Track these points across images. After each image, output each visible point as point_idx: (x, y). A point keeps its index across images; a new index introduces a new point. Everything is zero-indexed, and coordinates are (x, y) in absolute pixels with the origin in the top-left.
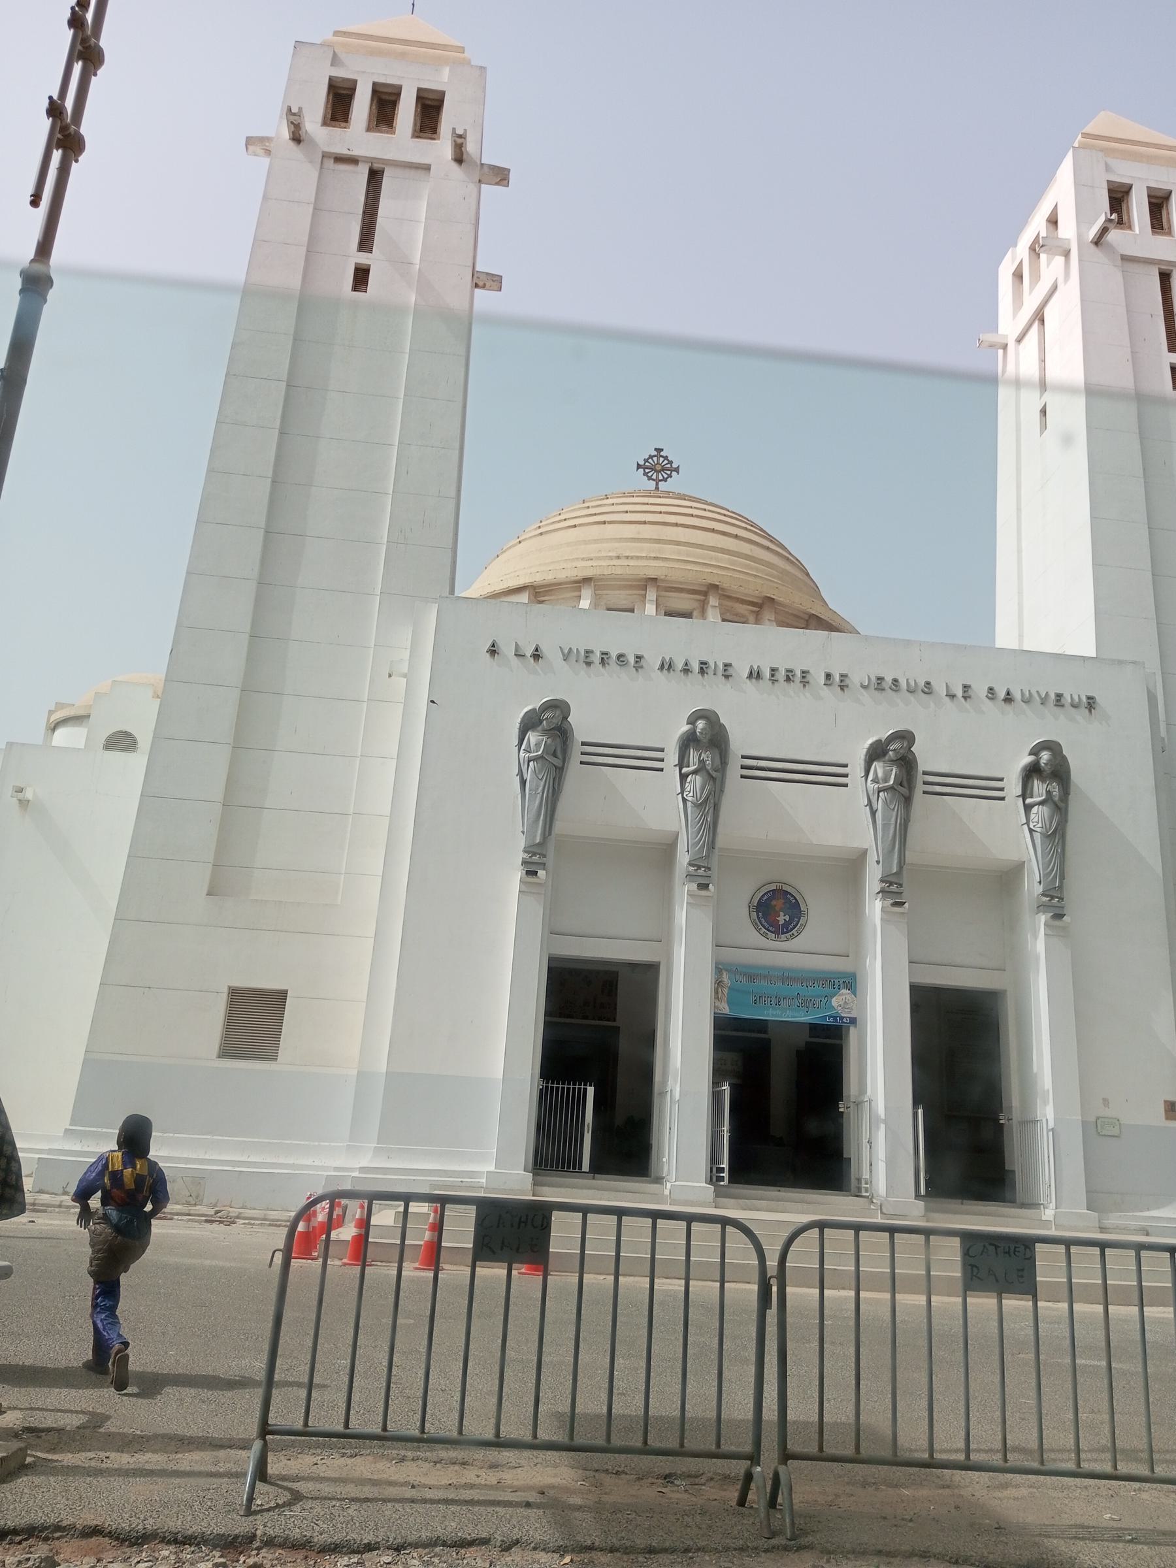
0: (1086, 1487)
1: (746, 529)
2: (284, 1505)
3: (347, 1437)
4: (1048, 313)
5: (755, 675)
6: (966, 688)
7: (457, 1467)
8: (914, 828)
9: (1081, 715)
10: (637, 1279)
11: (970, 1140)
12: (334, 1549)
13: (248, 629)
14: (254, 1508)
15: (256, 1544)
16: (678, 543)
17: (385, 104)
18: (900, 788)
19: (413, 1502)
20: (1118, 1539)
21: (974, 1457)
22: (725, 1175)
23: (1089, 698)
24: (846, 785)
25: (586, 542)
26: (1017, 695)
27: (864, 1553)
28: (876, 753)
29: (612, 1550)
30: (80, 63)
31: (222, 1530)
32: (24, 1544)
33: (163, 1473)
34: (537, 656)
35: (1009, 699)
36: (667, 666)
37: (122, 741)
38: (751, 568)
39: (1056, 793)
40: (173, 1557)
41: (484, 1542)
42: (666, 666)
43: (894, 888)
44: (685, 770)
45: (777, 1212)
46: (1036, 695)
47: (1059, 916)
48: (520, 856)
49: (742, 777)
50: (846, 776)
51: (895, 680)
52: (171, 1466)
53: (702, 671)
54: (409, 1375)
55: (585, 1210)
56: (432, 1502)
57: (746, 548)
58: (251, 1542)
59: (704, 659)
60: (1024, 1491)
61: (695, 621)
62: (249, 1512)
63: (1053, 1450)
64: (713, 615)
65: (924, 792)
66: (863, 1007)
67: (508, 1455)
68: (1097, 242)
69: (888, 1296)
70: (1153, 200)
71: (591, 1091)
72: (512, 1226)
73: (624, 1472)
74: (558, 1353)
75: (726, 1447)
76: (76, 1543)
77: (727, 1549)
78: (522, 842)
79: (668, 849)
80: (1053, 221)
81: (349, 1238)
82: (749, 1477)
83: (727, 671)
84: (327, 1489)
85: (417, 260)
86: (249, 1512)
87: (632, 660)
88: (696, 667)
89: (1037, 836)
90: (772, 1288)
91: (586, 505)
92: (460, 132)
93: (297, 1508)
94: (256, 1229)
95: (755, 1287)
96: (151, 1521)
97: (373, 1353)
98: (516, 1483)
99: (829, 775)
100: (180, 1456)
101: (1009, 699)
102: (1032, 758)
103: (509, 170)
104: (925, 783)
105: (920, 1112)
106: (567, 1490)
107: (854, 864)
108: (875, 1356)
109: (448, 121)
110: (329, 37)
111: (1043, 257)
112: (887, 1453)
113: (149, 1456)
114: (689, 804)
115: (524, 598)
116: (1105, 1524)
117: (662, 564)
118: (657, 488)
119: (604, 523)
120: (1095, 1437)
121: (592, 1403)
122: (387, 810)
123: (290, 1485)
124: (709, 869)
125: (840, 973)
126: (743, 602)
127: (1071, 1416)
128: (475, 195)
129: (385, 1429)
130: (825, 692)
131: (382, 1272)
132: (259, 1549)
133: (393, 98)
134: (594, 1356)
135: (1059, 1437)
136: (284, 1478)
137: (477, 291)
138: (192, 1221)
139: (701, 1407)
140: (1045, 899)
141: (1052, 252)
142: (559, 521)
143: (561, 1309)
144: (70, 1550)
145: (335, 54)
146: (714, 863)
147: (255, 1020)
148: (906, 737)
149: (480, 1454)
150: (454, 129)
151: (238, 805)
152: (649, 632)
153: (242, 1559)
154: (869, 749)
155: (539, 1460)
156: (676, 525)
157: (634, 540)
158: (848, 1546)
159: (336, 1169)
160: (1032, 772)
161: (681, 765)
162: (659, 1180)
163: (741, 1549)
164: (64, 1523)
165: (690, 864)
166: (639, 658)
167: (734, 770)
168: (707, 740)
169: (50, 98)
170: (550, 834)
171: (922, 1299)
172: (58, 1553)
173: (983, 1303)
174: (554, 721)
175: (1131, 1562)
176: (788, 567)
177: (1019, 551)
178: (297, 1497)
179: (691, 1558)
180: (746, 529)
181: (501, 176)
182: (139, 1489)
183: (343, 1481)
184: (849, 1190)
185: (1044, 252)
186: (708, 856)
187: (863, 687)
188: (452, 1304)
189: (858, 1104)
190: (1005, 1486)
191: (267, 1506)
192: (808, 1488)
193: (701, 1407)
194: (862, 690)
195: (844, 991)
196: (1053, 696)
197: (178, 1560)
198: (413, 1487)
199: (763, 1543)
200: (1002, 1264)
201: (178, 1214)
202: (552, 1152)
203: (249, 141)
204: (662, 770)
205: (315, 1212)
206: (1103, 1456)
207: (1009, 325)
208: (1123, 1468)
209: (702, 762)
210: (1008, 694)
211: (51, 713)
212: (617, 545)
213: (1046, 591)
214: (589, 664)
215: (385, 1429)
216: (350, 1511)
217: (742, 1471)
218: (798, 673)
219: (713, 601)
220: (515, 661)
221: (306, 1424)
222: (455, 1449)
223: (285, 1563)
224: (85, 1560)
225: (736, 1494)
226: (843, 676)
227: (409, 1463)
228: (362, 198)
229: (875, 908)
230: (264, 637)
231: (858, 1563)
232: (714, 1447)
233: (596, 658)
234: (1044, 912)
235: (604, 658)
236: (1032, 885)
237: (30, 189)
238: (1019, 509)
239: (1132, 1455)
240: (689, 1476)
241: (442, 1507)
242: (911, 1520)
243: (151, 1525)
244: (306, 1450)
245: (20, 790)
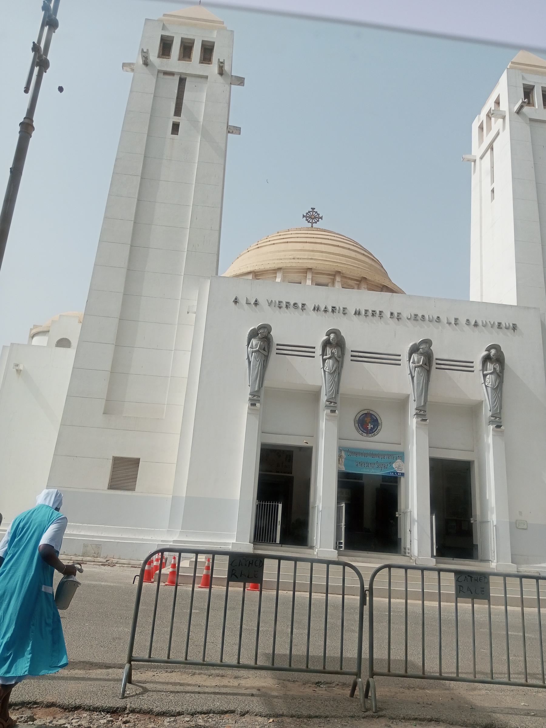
0: (512, 691)
1: (354, 245)
2: (139, 694)
3: (169, 663)
4: (495, 145)
5: (357, 313)
6: (456, 319)
7: (219, 678)
8: (432, 384)
9: (510, 333)
10: (302, 593)
11: (456, 531)
12: (163, 714)
13: (123, 291)
14: (125, 695)
15: (127, 711)
16: (322, 252)
17: (187, 49)
18: (425, 366)
19: (199, 693)
20: (528, 714)
21: (460, 675)
22: (343, 545)
23: (514, 324)
24: (400, 365)
25: (279, 251)
26: (480, 323)
27: (409, 719)
28: (414, 350)
29: (292, 716)
30: (47, 27)
31: (111, 705)
32: (20, 710)
33: (83, 679)
34: (256, 303)
35: (476, 325)
36: (316, 309)
37: (64, 343)
38: (355, 263)
39: (498, 369)
40: (88, 717)
41: (233, 712)
42: (316, 309)
43: (422, 413)
44: (325, 357)
45: (368, 562)
46: (489, 323)
47: (499, 427)
48: (248, 396)
49: (352, 360)
50: (400, 360)
51: (423, 316)
52: (86, 676)
53: (333, 311)
54: (197, 636)
55: (280, 558)
56: (208, 693)
57: (353, 254)
58: (124, 711)
59: (334, 306)
60: (484, 692)
61: (330, 288)
62: (123, 697)
63: (496, 673)
64: (338, 285)
65: (436, 368)
66: (407, 468)
67: (243, 673)
68: (518, 112)
69: (421, 602)
70: (544, 93)
71: (280, 506)
72: (246, 565)
73: (297, 681)
74: (267, 628)
75: (345, 669)
76: (44, 710)
77: (345, 716)
78: (249, 390)
79: (315, 395)
80: (497, 103)
81: (168, 573)
82: (355, 685)
83: (345, 311)
84: (159, 687)
85: (202, 120)
86: (123, 697)
87: (300, 306)
88: (330, 309)
89: (489, 389)
90: (366, 595)
91: (279, 234)
92: (221, 60)
93: (145, 696)
94: (126, 568)
95: (359, 597)
96: (78, 700)
97: (181, 626)
98: (247, 685)
99: (392, 360)
100: (90, 671)
101: (476, 325)
102: (487, 352)
103: (244, 78)
104: (437, 364)
105: (434, 517)
106: (270, 689)
107: (403, 403)
108: (415, 630)
109: (216, 56)
110: (161, 16)
111: (493, 119)
112: (420, 673)
113: (77, 671)
114: (327, 373)
115: (250, 277)
116: (521, 708)
117: (314, 262)
118: (312, 226)
119: (288, 242)
120: (517, 667)
121: (282, 649)
122: (186, 375)
123: (142, 685)
124: (336, 403)
125: (397, 452)
126: (352, 279)
127: (505, 657)
128: (228, 89)
129: (186, 659)
130: (391, 321)
131: (185, 589)
132: (128, 714)
133: (190, 45)
134: (284, 627)
135: (500, 668)
136: (139, 682)
137: (229, 134)
138: (94, 564)
139: (333, 652)
140: (492, 418)
141: (497, 117)
142: (267, 242)
143: (268, 607)
144: (41, 713)
145: (164, 24)
146: (338, 400)
147: (124, 473)
148: (428, 342)
149: (229, 672)
150: (219, 59)
151: (117, 374)
152: (309, 293)
153: (120, 718)
154: (410, 348)
155: (258, 675)
156: (321, 243)
157: (301, 250)
158: (402, 716)
159: (162, 541)
160: (487, 359)
161: (323, 355)
162: (312, 547)
163: (352, 717)
164: (38, 701)
165: (327, 401)
166: (303, 305)
167: (348, 357)
168: (335, 343)
169: (34, 43)
170: (262, 386)
171: (436, 604)
172: (35, 714)
173: (465, 605)
174: (264, 334)
175: (534, 725)
176: (373, 263)
177: (481, 256)
178: (145, 690)
179: (329, 720)
180: (354, 245)
181: (240, 81)
182: (72, 686)
183: (168, 683)
184: (400, 553)
185: (493, 117)
186: (335, 397)
187: (408, 319)
188: (217, 604)
189: (405, 513)
190: (475, 689)
191: (131, 695)
192: (383, 689)
193: (333, 652)
194: (408, 320)
195: (398, 460)
196: (497, 324)
197: (91, 718)
198: (199, 686)
199: (362, 714)
200: (473, 586)
201: (89, 561)
202: (261, 534)
203: (124, 65)
204: (314, 357)
205: (152, 560)
206: (520, 676)
207: (477, 150)
208: (530, 681)
209: (332, 353)
210: (476, 322)
211: (31, 329)
212: (293, 253)
213: (493, 277)
214: (280, 307)
215: (186, 659)
216: (170, 697)
217: (352, 682)
218: (378, 312)
219: (338, 279)
220: (246, 306)
221: (150, 657)
222: (218, 669)
223: (140, 720)
224: (48, 718)
225: (349, 692)
226: (399, 314)
227: (197, 676)
228: (176, 91)
229: (413, 422)
230: (130, 295)
231: (406, 724)
232: (339, 669)
233: (284, 305)
234: (492, 424)
235: (288, 305)
236: (487, 412)
237: (24, 84)
238: (481, 237)
239: (534, 676)
240: (327, 683)
241: (213, 696)
242: (431, 705)
243: (78, 702)
244: (149, 669)
245: (17, 365)
